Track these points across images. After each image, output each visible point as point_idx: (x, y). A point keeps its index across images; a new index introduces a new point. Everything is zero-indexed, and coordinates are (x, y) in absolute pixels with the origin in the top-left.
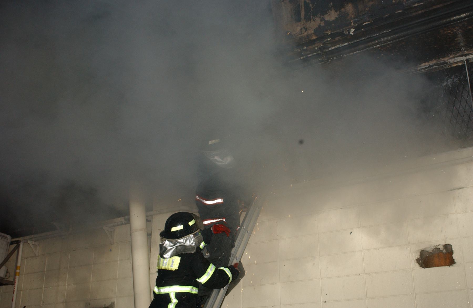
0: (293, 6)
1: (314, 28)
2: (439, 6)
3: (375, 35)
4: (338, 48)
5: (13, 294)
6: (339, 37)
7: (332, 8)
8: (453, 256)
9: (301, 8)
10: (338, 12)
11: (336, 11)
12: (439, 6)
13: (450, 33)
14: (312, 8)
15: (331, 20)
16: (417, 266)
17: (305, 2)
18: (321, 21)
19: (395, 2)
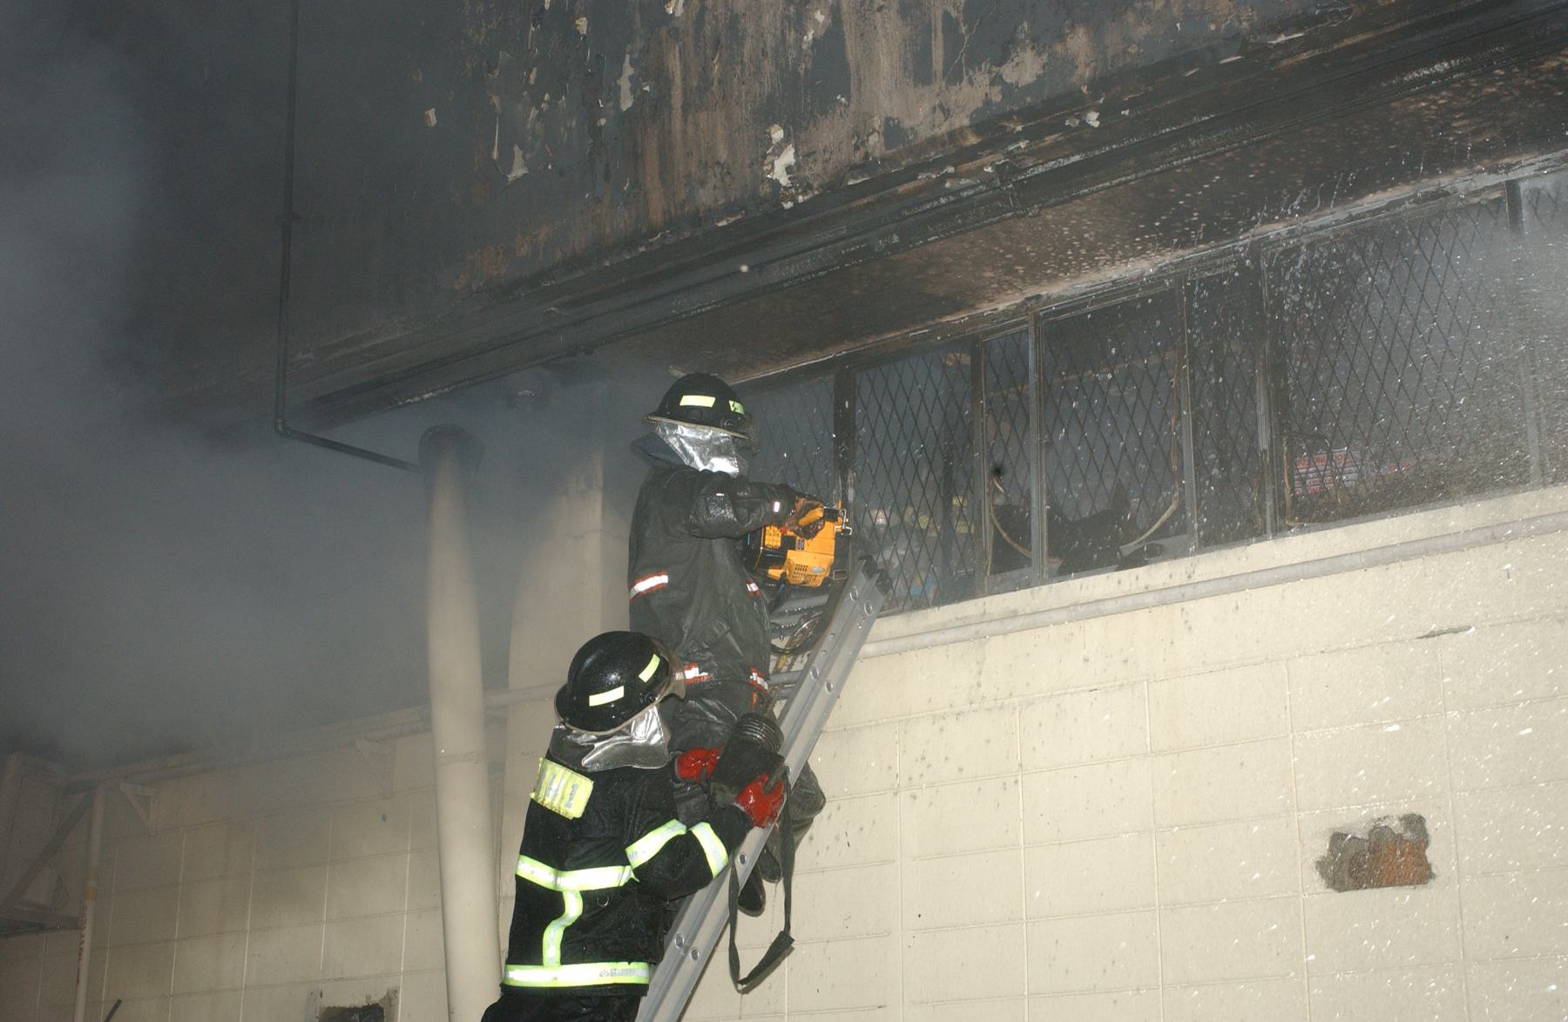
0: (909, 28)
1: (971, 110)
2: (1360, 38)
3: (1168, 130)
4: (1052, 171)
5: (80, 960)
6: (1056, 136)
7: (1028, 41)
8: (1428, 852)
9: (933, 35)
10: (1045, 57)
11: (1040, 54)
12: (1360, 38)
13: (1429, 109)
14: (966, 38)
15: (1023, 84)
16: (1316, 881)
17: (946, 15)
18: (992, 84)
19: (1216, 29)
